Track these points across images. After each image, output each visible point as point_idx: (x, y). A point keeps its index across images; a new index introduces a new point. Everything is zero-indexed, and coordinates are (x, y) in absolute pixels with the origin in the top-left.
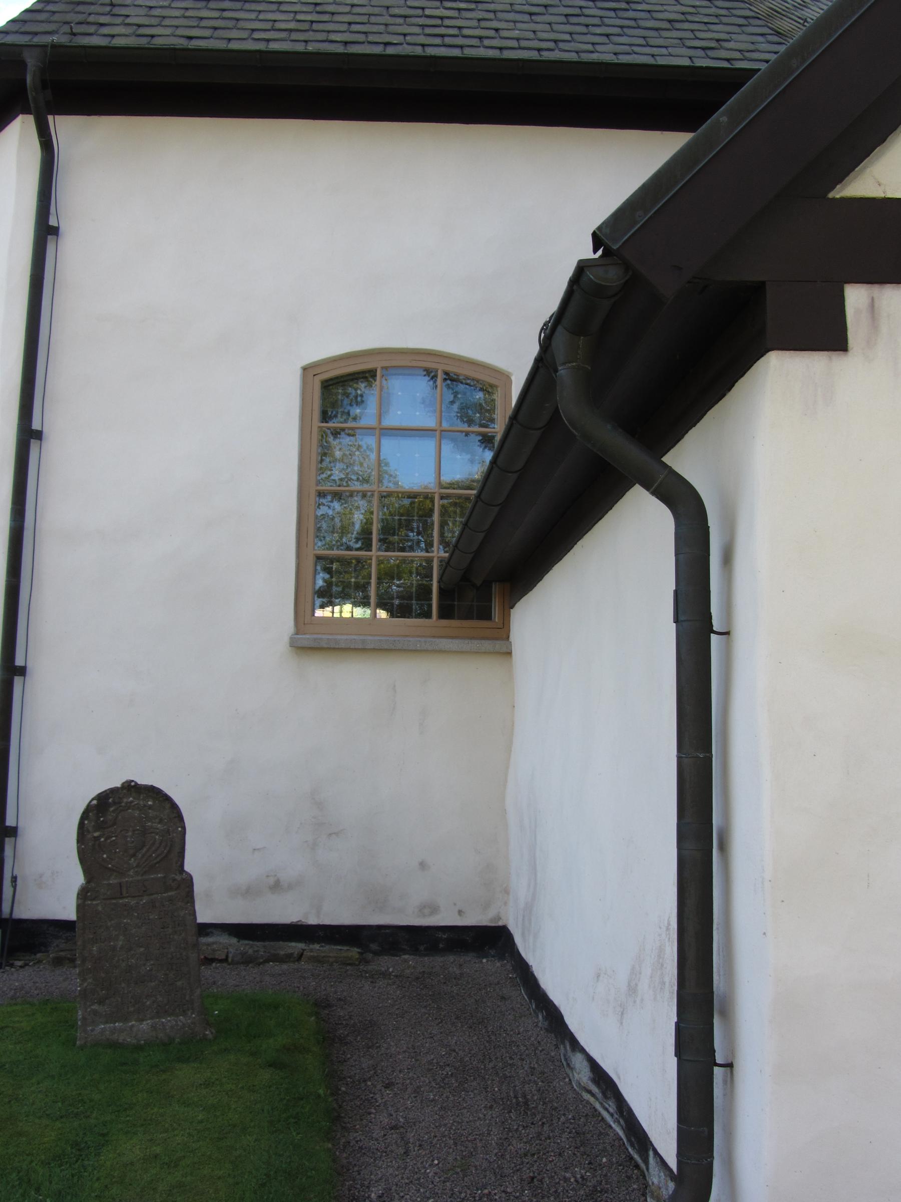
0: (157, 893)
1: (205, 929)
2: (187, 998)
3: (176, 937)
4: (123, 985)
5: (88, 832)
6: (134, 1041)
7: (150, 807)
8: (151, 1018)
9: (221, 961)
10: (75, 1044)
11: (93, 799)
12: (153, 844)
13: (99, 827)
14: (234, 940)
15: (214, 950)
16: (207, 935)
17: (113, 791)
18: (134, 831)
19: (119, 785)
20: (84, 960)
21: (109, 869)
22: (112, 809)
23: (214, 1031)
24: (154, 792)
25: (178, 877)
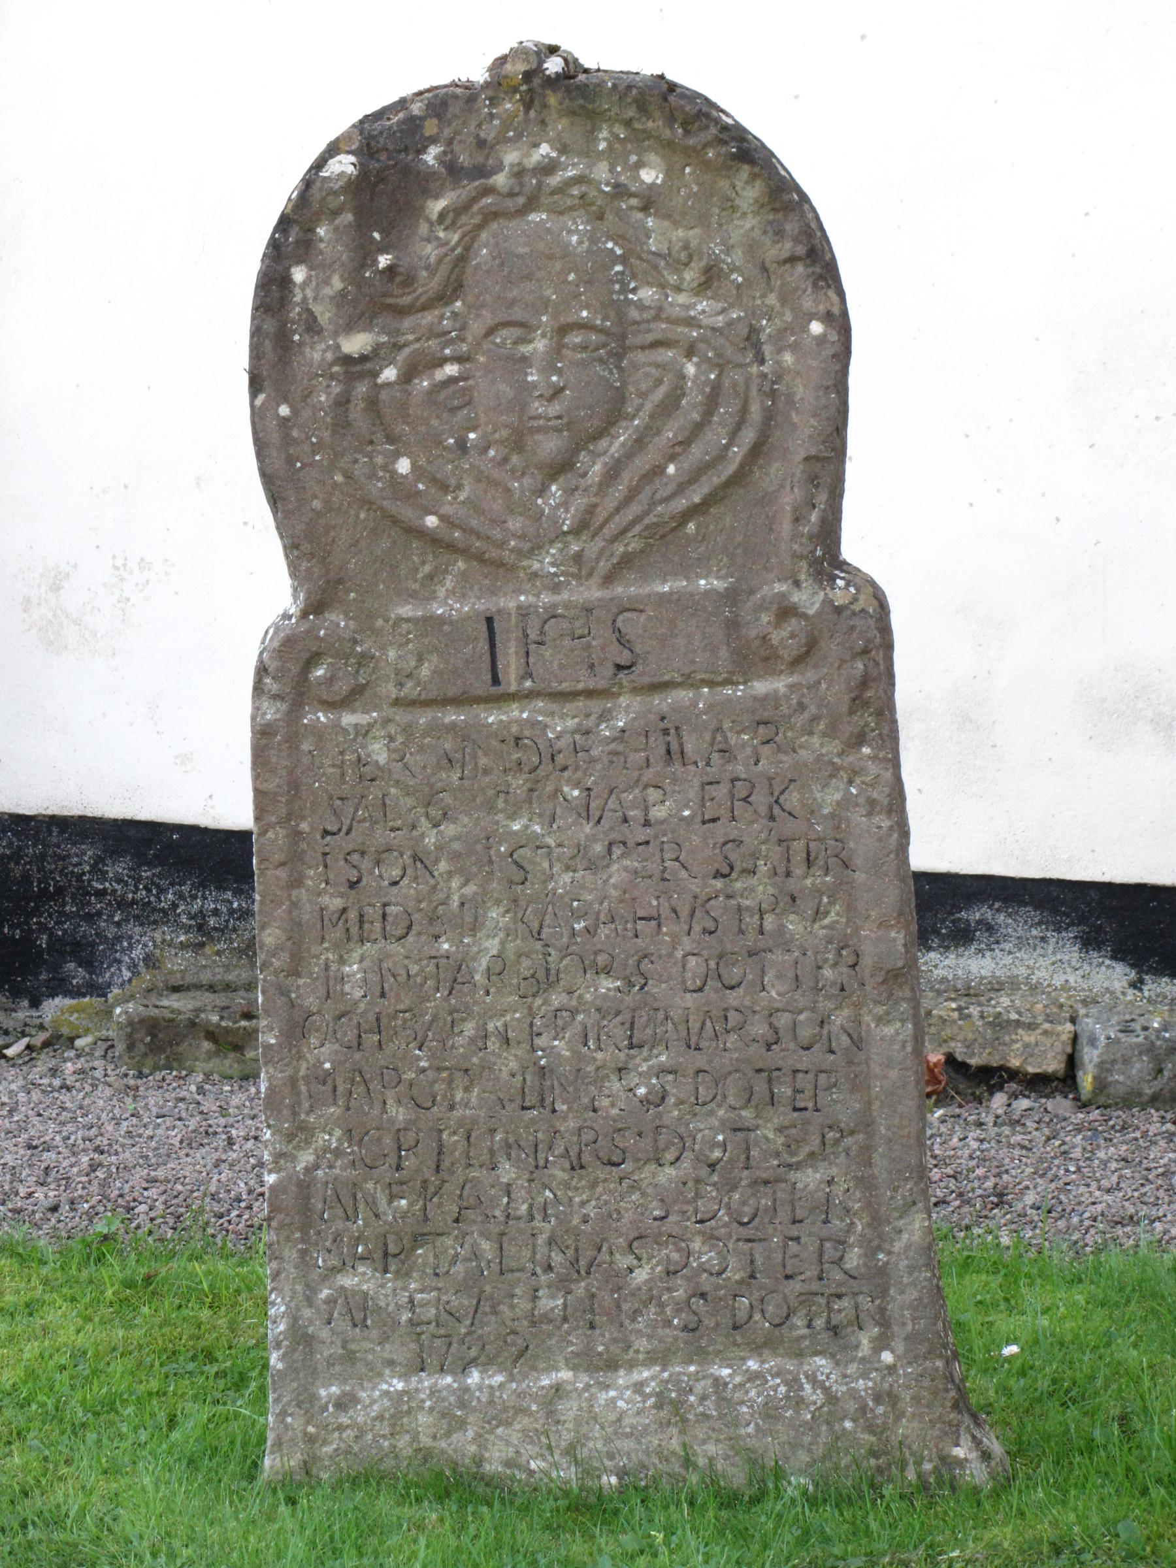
0: (688, 681)
1: (951, 905)
2: (853, 1259)
3: (793, 925)
4: (507, 1172)
5: (312, 326)
6: (568, 1474)
7: (649, 201)
8: (652, 1358)
9: (1038, 1084)
10: (252, 1471)
11: (333, 150)
13: (374, 301)
14: (1112, 976)
15: (1000, 1024)
16: (962, 937)
17: (445, 103)
20: (297, 1029)
22: (437, 206)
23: (997, 1448)
24: (670, 114)
25: (809, 599)
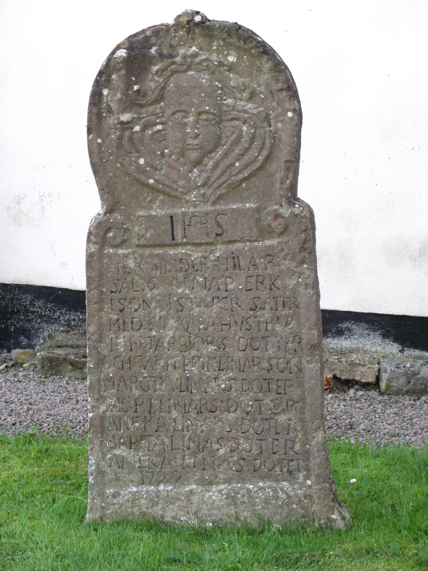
0: (242, 240)
1: (335, 322)
2: (297, 447)
3: (278, 328)
4: (175, 414)
5: (110, 111)
6: (195, 522)
7: (231, 68)
8: (228, 481)
9: (366, 386)
10: (158, 301)
11: (118, 47)
12: (237, 142)
13: (132, 102)
14: (393, 348)
15: (352, 364)
16: (340, 333)
17: (158, 31)
18: (199, 114)
19: (171, 22)
20: (101, 362)
21: (148, 186)
22: (155, 68)
25: (285, 211)
